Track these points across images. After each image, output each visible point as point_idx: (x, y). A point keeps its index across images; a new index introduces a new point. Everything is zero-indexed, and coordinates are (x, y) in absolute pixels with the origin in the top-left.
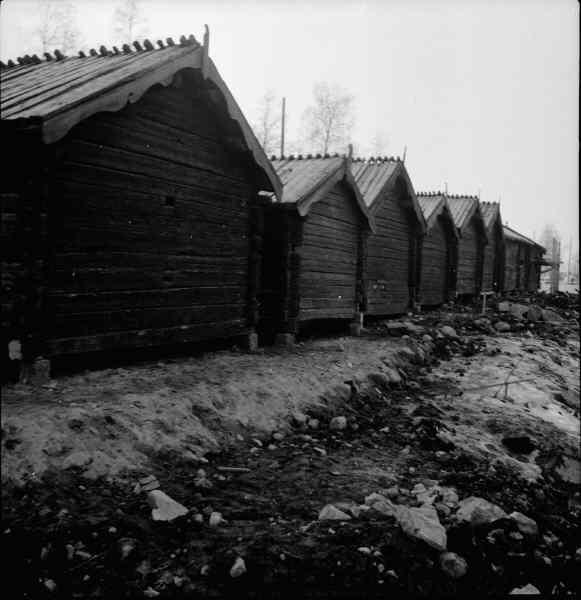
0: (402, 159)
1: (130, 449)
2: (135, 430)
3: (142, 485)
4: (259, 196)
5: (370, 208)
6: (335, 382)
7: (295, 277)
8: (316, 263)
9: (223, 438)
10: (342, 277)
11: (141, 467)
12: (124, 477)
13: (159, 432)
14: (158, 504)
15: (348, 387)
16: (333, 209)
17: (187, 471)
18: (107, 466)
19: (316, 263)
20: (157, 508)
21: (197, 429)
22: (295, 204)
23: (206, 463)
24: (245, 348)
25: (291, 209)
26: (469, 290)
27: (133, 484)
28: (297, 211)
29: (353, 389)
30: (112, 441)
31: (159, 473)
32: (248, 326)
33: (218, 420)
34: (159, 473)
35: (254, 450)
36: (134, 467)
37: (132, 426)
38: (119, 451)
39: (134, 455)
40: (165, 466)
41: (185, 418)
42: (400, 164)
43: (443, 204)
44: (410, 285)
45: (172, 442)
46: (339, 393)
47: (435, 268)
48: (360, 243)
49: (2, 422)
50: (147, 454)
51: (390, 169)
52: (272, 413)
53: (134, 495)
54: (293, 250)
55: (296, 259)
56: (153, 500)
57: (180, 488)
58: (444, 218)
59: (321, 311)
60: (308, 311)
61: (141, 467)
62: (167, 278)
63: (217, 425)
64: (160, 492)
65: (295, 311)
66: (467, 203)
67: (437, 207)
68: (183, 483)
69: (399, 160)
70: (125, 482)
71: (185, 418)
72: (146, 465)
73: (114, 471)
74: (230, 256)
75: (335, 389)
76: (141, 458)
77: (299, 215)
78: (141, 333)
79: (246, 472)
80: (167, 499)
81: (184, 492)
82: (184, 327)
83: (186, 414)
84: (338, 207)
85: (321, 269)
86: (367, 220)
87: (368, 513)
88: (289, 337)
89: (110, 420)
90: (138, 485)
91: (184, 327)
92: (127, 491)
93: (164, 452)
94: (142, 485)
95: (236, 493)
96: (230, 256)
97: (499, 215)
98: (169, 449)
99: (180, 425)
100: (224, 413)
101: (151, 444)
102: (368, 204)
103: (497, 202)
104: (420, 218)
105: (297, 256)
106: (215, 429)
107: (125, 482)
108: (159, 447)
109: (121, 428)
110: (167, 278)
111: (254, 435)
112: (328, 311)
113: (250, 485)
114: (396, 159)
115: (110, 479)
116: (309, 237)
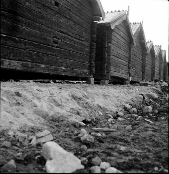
0: (141, 23)
1: (31, 112)
2: (36, 101)
3: (37, 138)
4: (94, 23)
5: (134, 35)
6: (135, 95)
7: (109, 56)
8: (116, 53)
9: (91, 113)
10: (124, 62)
11: (38, 125)
12: (24, 131)
13: (52, 104)
14: (52, 154)
15: (142, 97)
16: (121, 33)
17: (72, 130)
18: (11, 122)
19: (116, 53)
20: (51, 159)
21: (74, 105)
22: (109, 23)
23: (84, 126)
24: (88, 82)
25: (106, 27)
26: (157, 79)
27: (30, 137)
28: (110, 26)
29: (144, 98)
30: (17, 107)
31: (53, 130)
32: (91, 74)
33: (87, 103)
34: (53, 130)
35: (110, 120)
36: (32, 125)
37: (33, 98)
38: (23, 114)
39: (34, 117)
40: (56, 126)
41: (68, 100)
42: (141, 25)
43: (152, 45)
44: (143, 72)
45: (63, 112)
46: (137, 100)
47: (149, 68)
48: (130, 49)
49: (33, 172)
50: (44, 117)
51: (138, 26)
52: (113, 104)
53: (30, 147)
54: (108, 44)
55: (109, 48)
56: (48, 150)
57: (68, 140)
58: (152, 51)
59: (117, 73)
60: (114, 72)
61: (38, 125)
62: (55, 42)
63: (87, 106)
64: (54, 142)
65: (109, 70)
66: (157, 48)
67: (150, 46)
68: (71, 138)
69: (140, 23)
70: (24, 135)
71: (68, 100)
72: (43, 124)
73: (15, 127)
74: (82, 40)
75: (136, 97)
76: (39, 119)
77: (111, 28)
78: (43, 66)
79: (113, 131)
80: (60, 149)
81: (74, 145)
82: (63, 68)
83: (68, 98)
84: (123, 32)
85: (117, 56)
86: (133, 40)
87: (150, 164)
88: (107, 81)
89: (18, 94)
90: (34, 138)
91: (63, 68)
92: (26, 143)
93: (55, 117)
94: (37, 138)
95: (114, 146)
96: (82, 40)
97: (165, 54)
98: (59, 115)
99: (66, 103)
100: (89, 101)
101: (47, 110)
102: (133, 34)
103: (165, 50)
104: (146, 47)
105: (110, 46)
106: (86, 108)
107: (24, 135)
108: (51, 113)
109: (26, 99)
110: (55, 42)
111: (107, 112)
112: (119, 74)
113: (121, 140)
114: (139, 23)
115: (11, 133)
116: (113, 41)
